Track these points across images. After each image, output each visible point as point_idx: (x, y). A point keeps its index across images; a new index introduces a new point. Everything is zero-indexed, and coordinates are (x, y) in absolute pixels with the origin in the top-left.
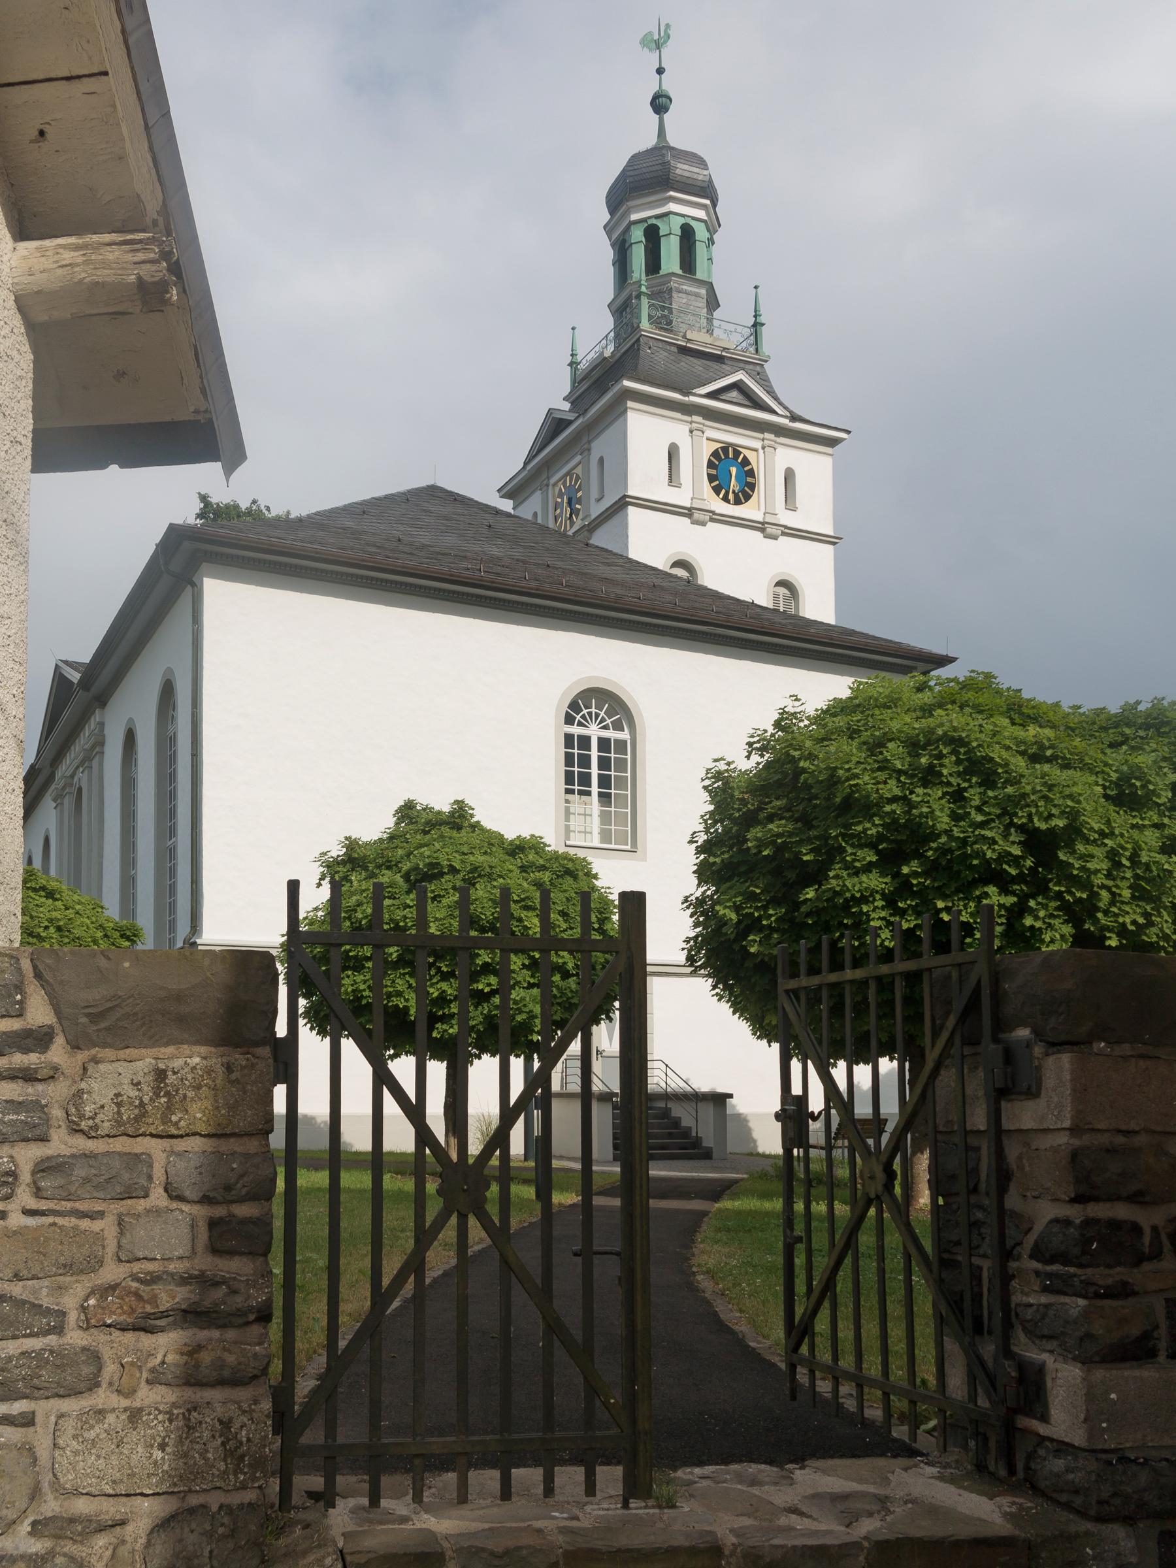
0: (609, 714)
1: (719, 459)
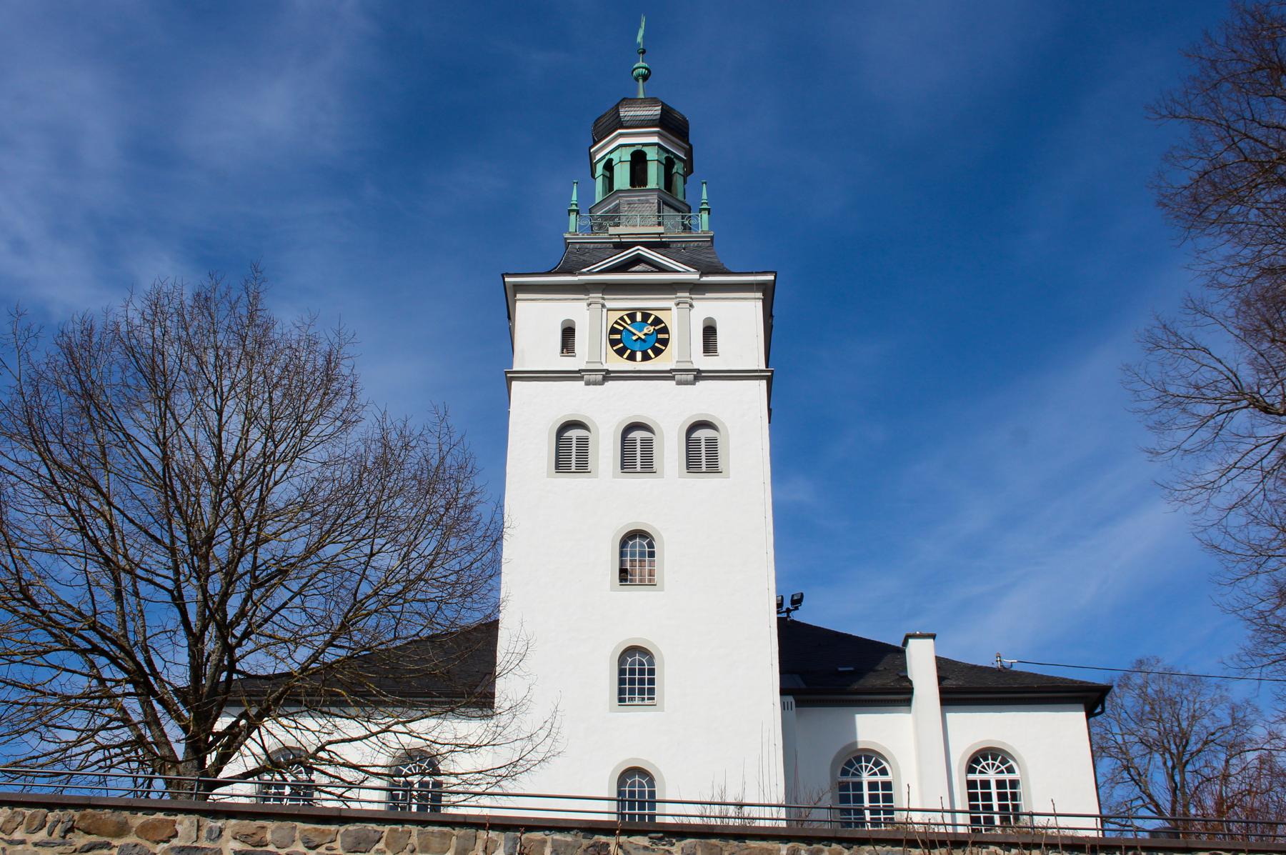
1: (619, 341)
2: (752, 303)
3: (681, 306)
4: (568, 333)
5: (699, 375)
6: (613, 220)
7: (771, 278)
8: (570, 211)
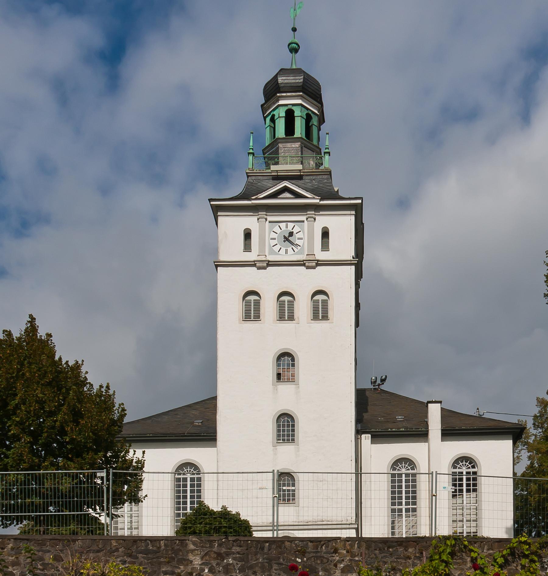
0: (470, 463)
2: (348, 218)
3: (309, 219)
4: (248, 235)
5: (319, 263)
6: (274, 160)
7: (360, 201)
8: (249, 153)
